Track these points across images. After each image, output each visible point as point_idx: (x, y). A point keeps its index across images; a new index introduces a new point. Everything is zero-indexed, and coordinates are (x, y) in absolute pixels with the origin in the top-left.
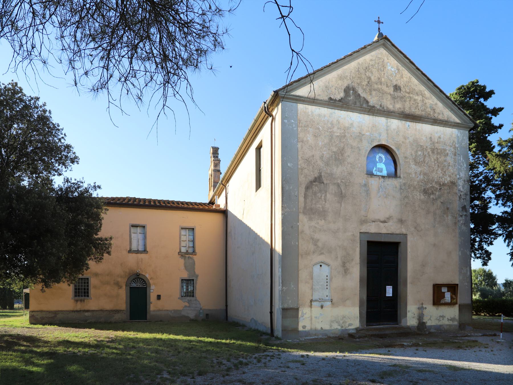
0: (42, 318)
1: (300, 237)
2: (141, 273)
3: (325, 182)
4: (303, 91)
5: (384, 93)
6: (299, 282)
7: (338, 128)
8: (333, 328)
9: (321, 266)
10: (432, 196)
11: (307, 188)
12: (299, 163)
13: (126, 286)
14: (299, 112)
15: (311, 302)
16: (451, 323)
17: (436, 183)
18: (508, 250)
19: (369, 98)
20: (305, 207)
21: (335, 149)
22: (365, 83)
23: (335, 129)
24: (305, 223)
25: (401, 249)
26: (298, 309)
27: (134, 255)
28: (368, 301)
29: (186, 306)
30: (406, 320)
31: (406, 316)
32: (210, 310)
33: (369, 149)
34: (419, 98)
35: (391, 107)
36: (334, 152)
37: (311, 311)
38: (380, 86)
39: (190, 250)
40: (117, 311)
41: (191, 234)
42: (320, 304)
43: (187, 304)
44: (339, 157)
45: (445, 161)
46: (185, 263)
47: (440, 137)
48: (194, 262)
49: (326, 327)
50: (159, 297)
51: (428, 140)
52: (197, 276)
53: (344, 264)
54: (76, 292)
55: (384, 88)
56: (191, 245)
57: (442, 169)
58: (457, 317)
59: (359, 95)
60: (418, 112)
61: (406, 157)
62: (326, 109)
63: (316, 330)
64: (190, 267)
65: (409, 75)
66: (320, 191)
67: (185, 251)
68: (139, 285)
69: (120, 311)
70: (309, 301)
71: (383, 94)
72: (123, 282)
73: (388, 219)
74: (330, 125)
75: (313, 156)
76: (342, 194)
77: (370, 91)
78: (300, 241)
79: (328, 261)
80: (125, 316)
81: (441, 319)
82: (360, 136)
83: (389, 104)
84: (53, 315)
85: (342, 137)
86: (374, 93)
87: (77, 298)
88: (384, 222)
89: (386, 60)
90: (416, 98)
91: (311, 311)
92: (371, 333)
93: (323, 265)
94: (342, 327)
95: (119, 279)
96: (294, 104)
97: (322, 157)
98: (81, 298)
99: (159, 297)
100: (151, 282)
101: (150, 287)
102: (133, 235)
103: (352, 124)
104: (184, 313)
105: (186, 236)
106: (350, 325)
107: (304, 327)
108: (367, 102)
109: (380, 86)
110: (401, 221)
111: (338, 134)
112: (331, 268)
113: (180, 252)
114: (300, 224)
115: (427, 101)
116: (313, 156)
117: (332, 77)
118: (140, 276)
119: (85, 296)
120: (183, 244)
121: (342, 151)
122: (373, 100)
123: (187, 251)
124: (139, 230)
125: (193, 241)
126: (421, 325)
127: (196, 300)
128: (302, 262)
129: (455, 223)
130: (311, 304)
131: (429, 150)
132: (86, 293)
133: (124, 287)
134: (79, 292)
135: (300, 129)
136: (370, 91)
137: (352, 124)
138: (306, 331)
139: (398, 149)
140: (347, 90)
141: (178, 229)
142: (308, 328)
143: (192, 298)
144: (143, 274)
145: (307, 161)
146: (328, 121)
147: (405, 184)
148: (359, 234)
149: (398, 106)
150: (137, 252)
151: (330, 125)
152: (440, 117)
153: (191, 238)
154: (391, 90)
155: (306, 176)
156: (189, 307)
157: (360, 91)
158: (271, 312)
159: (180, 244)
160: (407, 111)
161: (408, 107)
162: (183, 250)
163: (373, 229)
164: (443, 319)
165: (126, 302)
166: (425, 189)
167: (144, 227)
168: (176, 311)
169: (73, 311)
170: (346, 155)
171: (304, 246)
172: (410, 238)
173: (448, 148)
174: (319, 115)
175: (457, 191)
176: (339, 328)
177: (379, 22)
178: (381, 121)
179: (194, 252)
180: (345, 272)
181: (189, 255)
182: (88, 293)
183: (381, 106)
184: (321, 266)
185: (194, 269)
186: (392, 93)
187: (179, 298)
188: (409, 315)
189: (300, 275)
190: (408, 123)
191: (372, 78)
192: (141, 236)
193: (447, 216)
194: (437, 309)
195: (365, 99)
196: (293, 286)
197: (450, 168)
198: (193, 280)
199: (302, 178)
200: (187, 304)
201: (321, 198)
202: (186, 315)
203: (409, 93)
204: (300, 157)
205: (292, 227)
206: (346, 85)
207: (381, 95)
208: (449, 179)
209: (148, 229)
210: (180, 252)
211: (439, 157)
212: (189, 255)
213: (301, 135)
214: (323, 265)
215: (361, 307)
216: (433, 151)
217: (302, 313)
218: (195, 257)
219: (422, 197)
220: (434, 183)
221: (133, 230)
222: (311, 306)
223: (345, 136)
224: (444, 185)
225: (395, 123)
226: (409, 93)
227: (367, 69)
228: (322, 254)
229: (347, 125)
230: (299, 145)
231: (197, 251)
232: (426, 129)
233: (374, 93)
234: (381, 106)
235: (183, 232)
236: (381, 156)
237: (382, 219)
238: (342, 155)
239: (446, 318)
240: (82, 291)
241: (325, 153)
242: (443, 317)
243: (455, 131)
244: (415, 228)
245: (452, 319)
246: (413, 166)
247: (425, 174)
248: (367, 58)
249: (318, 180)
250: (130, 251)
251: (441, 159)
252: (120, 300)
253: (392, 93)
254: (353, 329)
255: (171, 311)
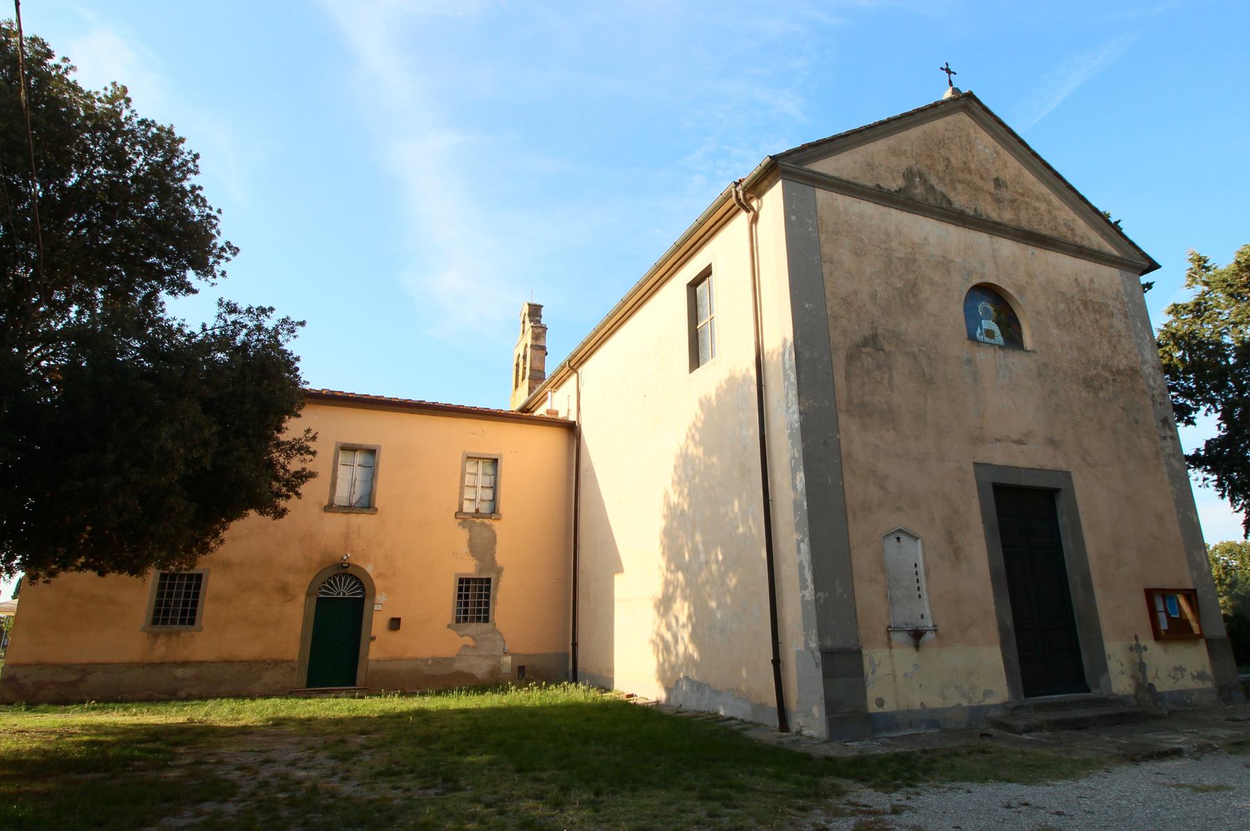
0: (41, 686)
1: (844, 467)
2: (353, 561)
3: (887, 348)
4: (824, 166)
5: (978, 189)
6: (855, 578)
7: (901, 244)
8: (949, 704)
9: (898, 539)
10: (1102, 394)
11: (851, 358)
12: (829, 304)
13: (308, 594)
14: (819, 204)
15: (889, 632)
16: (1198, 684)
17: (1105, 367)
18: (1242, 516)
19: (951, 195)
20: (850, 401)
21: (899, 284)
22: (940, 167)
23: (894, 245)
24: (855, 437)
25: (1061, 504)
26: (858, 653)
27: (340, 518)
28: (1019, 628)
29: (466, 646)
30: (1109, 679)
31: (1104, 669)
32: (529, 656)
33: (965, 290)
34: (1042, 206)
35: (994, 216)
36: (897, 289)
37: (891, 656)
38: (968, 177)
39: (485, 508)
40: (276, 663)
41: (490, 470)
42: (201, 645)
43: (468, 641)
44: (909, 297)
45: (1111, 326)
46: (470, 539)
47: (1092, 281)
48: (495, 536)
49: (934, 702)
50: (395, 624)
51: (1074, 284)
52: (499, 571)
53: (950, 538)
54: (157, 612)
55: (977, 179)
56: (488, 494)
57: (1110, 342)
58: (1209, 671)
59: (932, 187)
60: (1044, 231)
61: (1038, 313)
62: (872, 205)
63: (909, 711)
64: (483, 548)
65: (1018, 164)
66: (879, 367)
67: (473, 511)
68: (344, 591)
69: (282, 662)
70: (883, 630)
71: (976, 190)
72: (300, 584)
73: (1026, 435)
74: (883, 236)
75: (856, 293)
76: (924, 376)
77: (952, 182)
78: (847, 477)
79: (915, 528)
80: (301, 677)
81: (1179, 674)
82: (945, 264)
83: (990, 211)
84: (74, 677)
85: (909, 261)
86: (959, 187)
87: (156, 628)
88: (1020, 442)
89: (973, 134)
90: (1037, 205)
91: (891, 656)
92: (1042, 717)
93: (904, 538)
94: (970, 701)
95: (291, 578)
96: (809, 189)
97: (873, 297)
98: (165, 629)
99: (395, 624)
100: (378, 583)
101: (374, 595)
102: (341, 469)
103: (926, 239)
104: (459, 666)
105: (478, 476)
106: (987, 693)
107: (880, 702)
108: (950, 202)
109: (968, 177)
110: (1052, 442)
111: (902, 255)
112: (923, 546)
113: (461, 511)
114: (842, 436)
115: (1056, 213)
116: (856, 293)
117: (877, 148)
118: (350, 571)
119: (182, 622)
120: (469, 494)
121: (912, 289)
122: (960, 200)
123: (477, 510)
124: (359, 458)
125: (494, 488)
126: (1144, 687)
127: (494, 631)
128: (857, 532)
129: (1157, 453)
130: (890, 639)
131: (1078, 303)
132: (189, 616)
133: (302, 598)
134: (166, 612)
135: (823, 237)
136: (952, 182)
137: (926, 239)
138: (885, 714)
139: (1021, 294)
140: (909, 175)
141: (459, 459)
142: (889, 707)
143: (482, 627)
144: (359, 564)
145: (847, 302)
146: (879, 228)
147: (1046, 365)
148: (972, 467)
149: (1007, 216)
150: (349, 509)
151: (883, 236)
152: (1086, 243)
153: (488, 481)
154: (990, 186)
155: (844, 333)
156: (475, 647)
157: (933, 181)
158: (777, 662)
159: (462, 493)
160: (1024, 224)
161: (1025, 220)
162: (469, 508)
163: (999, 456)
164: (1183, 676)
165: (303, 638)
166: (1085, 379)
167: (372, 452)
168: (437, 661)
169: (140, 665)
170: (922, 296)
171: (855, 490)
172: (1077, 481)
173: (1110, 302)
174: (861, 215)
175: (1145, 387)
176: (965, 703)
177: (948, 71)
178: (982, 239)
179: (494, 511)
180: (957, 557)
181: (480, 521)
182: (193, 613)
183: (975, 211)
184: (898, 539)
185: (493, 553)
186: (992, 190)
187: (449, 626)
188: (1113, 666)
189: (855, 562)
190: (1031, 249)
191: (952, 159)
192: (359, 473)
193: (1139, 438)
194: (1166, 651)
195: (944, 196)
196: (840, 590)
197: (1123, 340)
198: (489, 580)
199: (836, 336)
200: (468, 641)
201: (881, 382)
202: (466, 670)
203: (1022, 195)
204: (828, 293)
205: (825, 443)
206: (905, 166)
207: (973, 192)
208: (1125, 362)
209: (384, 459)
210: (461, 511)
211: (1098, 317)
212: (480, 521)
213: (827, 249)
214: (904, 538)
215: (1004, 645)
216: (1085, 304)
217: (872, 662)
218: (496, 525)
219: (1084, 394)
220: (1100, 368)
221: (342, 457)
222: (889, 644)
223: (915, 260)
224: (1119, 372)
225: (1008, 247)
226: (1022, 195)
227: (941, 143)
228: (899, 509)
229: (917, 240)
230: (826, 270)
231: (503, 507)
232: (1067, 264)
233: (959, 187)
234: (975, 211)
235: (471, 467)
236: (984, 306)
237: (1015, 437)
238: (914, 296)
239: (1187, 674)
240: (178, 606)
241: (879, 289)
242: (1180, 669)
243: (346, 494)
244: (1083, 459)
245: (1201, 676)
246: (1055, 331)
247: (1080, 349)
248: (939, 125)
249: (872, 341)
250: (330, 507)
251: (1104, 322)
252: (288, 632)
253: (992, 190)
254: (995, 706)
255: (425, 661)
